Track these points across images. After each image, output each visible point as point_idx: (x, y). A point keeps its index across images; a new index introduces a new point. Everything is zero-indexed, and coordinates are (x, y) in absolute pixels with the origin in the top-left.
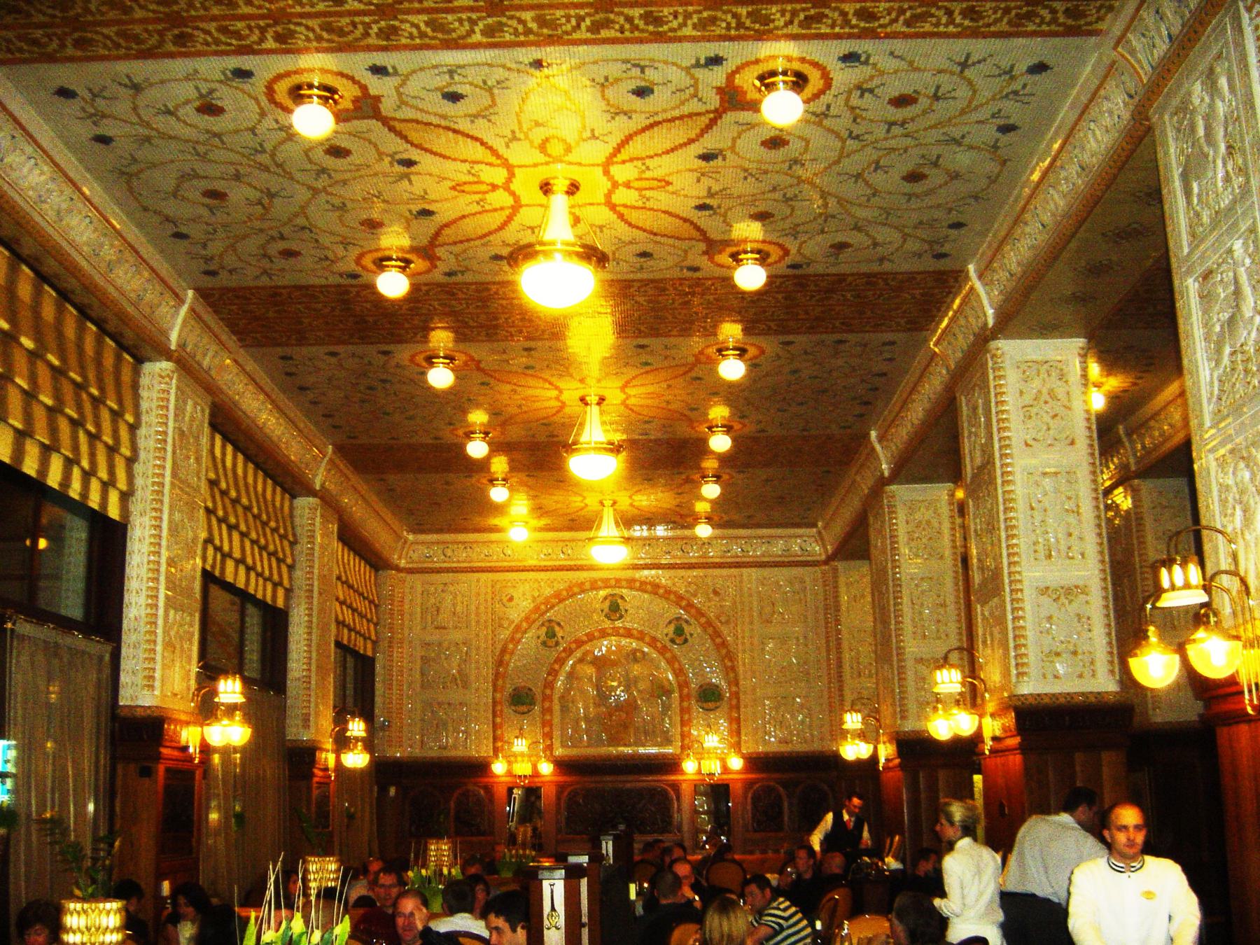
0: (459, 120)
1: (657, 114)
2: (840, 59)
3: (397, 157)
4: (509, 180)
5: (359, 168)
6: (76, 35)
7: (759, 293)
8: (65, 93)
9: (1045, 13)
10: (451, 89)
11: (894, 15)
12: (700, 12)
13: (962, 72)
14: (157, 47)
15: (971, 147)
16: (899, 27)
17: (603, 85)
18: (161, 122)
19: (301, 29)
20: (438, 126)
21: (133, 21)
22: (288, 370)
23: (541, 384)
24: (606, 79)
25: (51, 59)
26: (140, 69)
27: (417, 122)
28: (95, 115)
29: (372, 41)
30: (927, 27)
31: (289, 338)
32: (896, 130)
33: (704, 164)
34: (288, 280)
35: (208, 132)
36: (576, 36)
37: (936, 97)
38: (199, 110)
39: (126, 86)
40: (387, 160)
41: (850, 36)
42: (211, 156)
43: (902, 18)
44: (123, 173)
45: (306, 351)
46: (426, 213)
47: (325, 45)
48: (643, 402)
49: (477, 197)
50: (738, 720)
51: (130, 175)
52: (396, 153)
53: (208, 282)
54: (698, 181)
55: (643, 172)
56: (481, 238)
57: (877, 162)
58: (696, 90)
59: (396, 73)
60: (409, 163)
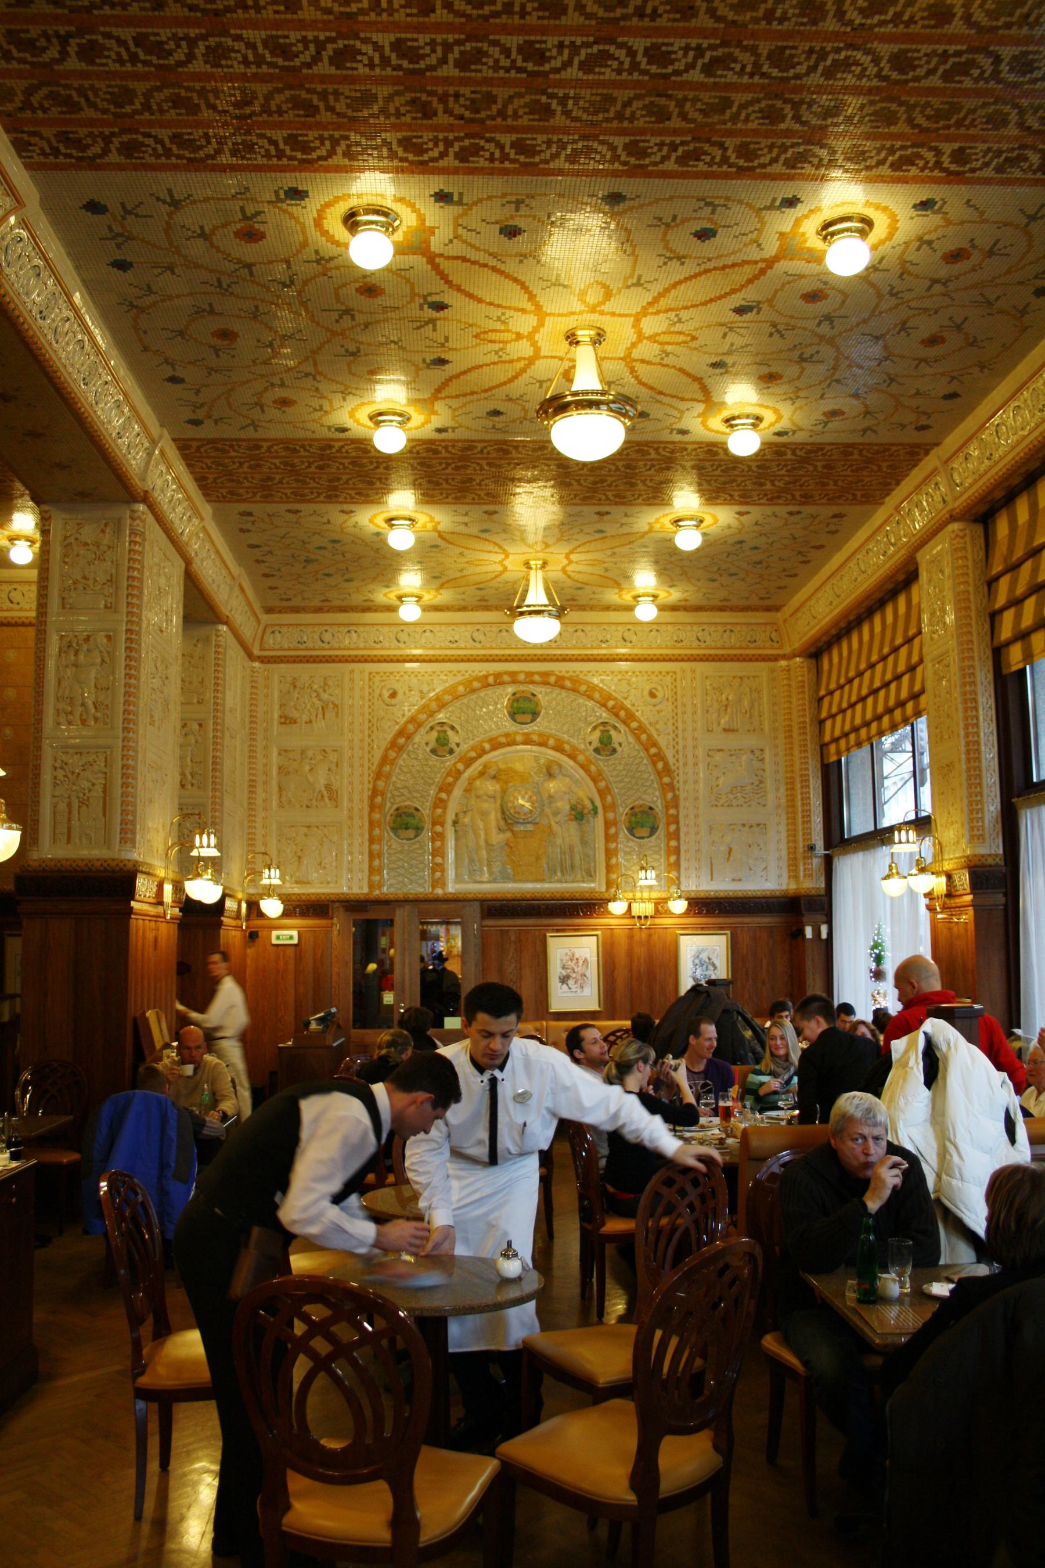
0: (508, 260)
1: (709, 260)
2: (915, 206)
3: (429, 299)
4: (536, 330)
5: (385, 309)
6: (125, 138)
7: (738, 460)
8: (94, 207)
9: (930, 155)
10: (511, 223)
11: (883, 155)
12: (575, 142)
13: (1027, 225)
14: (100, 156)
15: (1001, 312)
16: (670, 165)
17: (668, 225)
18: (197, 249)
19: (150, 141)
20: (485, 266)
21: (198, 124)
22: (245, 527)
23: (491, 547)
24: (675, 218)
25: (92, 164)
26: (180, 182)
27: (464, 259)
28: (121, 235)
29: (225, 159)
30: (701, 167)
31: (255, 494)
32: (938, 288)
33: (737, 318)
34: (275, 432)
35: (239, 261)
36: (441, 163)
37: (991, 253)
38: (237, 234)
39: (164, 202)
40: (419, 301)
41: (615, 174)
42: (236, 289)
43: (783, 157)
44: (132, 305)
45: (271, 508)
46: (442, 362)
47: (61, 159)
48: (590, 569)
49: (497, 346)
50: (677, 851)
51: (142, 310)
52: (430, 294)
53: (192, 432)
54: (447, 339)
55: (674, 324)
56: (486, 391)
57: (904, 323)
58: (759, 236)
59: (460, 203)
60: (441, 307)
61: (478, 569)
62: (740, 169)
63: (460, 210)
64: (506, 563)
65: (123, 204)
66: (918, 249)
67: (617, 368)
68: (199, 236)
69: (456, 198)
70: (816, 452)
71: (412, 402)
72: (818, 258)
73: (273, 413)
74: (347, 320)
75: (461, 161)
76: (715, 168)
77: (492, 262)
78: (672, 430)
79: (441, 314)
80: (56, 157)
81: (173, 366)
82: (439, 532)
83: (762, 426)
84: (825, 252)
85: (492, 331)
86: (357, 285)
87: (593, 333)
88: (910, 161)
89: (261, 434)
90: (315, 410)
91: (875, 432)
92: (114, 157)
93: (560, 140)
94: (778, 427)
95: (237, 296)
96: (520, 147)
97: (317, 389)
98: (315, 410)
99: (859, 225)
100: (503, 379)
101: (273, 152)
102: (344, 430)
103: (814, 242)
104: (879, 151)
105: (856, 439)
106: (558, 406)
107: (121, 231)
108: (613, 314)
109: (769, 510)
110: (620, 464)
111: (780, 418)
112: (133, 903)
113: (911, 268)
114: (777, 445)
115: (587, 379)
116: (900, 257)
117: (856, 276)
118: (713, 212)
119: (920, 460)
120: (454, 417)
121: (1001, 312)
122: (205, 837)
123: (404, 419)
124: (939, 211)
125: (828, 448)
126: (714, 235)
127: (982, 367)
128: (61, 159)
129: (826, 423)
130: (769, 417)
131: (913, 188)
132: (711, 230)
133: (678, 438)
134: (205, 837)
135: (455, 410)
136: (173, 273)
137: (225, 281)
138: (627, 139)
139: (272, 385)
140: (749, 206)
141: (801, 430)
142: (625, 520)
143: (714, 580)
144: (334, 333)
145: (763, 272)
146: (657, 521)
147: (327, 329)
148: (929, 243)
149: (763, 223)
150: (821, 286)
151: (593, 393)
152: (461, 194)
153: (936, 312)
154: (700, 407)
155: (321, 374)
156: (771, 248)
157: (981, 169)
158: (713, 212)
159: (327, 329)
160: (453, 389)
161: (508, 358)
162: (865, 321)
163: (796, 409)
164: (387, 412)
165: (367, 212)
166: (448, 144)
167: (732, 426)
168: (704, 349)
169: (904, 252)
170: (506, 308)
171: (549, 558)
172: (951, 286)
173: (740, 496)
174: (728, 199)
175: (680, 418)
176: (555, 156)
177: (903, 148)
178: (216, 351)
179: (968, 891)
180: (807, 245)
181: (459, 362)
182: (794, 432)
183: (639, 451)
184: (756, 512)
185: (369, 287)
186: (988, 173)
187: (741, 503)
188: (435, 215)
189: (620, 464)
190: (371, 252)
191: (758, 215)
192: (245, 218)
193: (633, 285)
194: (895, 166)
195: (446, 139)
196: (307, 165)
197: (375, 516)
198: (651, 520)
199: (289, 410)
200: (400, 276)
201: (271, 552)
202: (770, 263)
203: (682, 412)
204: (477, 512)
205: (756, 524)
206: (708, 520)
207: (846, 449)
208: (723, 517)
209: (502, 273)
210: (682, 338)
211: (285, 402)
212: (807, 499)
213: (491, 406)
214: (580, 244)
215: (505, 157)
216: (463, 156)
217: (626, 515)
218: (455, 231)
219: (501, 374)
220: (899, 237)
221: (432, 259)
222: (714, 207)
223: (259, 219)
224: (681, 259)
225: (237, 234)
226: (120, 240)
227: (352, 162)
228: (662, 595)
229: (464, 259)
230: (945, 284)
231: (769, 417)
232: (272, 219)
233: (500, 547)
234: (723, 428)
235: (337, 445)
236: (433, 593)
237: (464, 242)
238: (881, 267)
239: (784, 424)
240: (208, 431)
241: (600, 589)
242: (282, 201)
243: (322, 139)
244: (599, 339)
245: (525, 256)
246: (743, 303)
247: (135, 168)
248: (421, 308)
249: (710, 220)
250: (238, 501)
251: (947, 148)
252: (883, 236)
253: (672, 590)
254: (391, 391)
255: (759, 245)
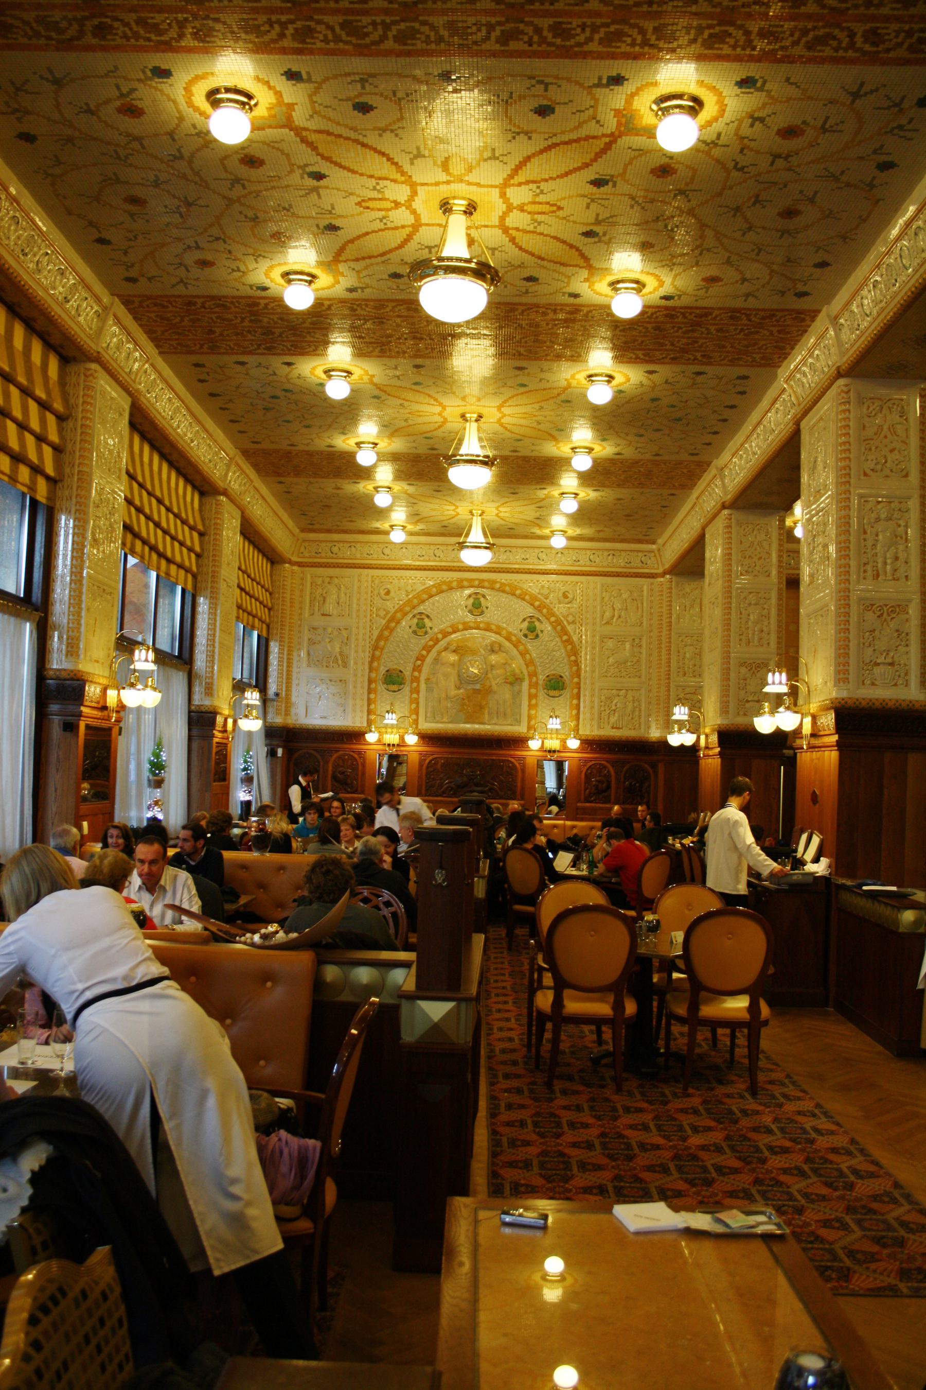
3: (308, 169)
13: (853, 102)
22: (202, 377)
23: (427, 400)
27: (329, 133)
31: (202, 346)
32: (780, 163)
38: (120, 110)
48: (523, 422)
52: (307, 165)
57: (758, 196)
58: (595, 112)
59: (309, 80)
60: (319, 176)
61: (420, 420)
62: (865, 53)
63: (310, 87)
64: (445, 414)
65: (13, 83)
66: (752, 126)
67: (494, 236)
68: (86, 112)
69: (305, 76)
70: (706, 315)
71: (320, 264)
72: (650, 133)
73: (196, 272)
74: (238, 188)
75: (502, 45)
76: (841, 53)
77: (353, 135)
78: (564, 294)
79: (322, 183)
80: (137, 40)
81: (97, 228)
82: (376, 385)
83: (645, 291)
84: (655, 127)
85: (370, 199)
86: (239, 156)
87: (465, 203)
88: (821, 41)
89: (192, 291)
90: (233, 270)
91: (186, 284)
92: (90, 39)
93: (593, 24)
94: (662, 292)
95: (136, 167)
96: (557, 30)
97: (230, 252)
98: (233, 270)
99: (691, 104)
100: (393, 245)
101: (330, 37)
102: (265, 289)
103: (648, 119)
104: (898, 33)
105: (739, 303)
106: (425, 267)
107: (16, 106)
108: (478, 185)
109: (677, 368)
110: (650, 326)
111: (661, 284)
112: (83, 708)
113: (752, 144)
114: (667, 308)
115: (456, 247)
116: (736, 134)
117: (691, 149)
118: (546, 90)
119: (809, 326)
120: (359, 278)
121: (848, 185)
122: (144, 652)
123: (640, 285)
124: (761, 89)
125: (716, 312)
126: (553, 112)
127: (844, 238)
128: (142, 42)
129: (708, 289)
130: (651, 283)
131: (735, 65)
132: (549, 106)
133: (572, 300)
134: (777, 674)
135: (358, 272)
136: (74, 145)
137: (122, 153)
138: (551, 21)
139: (189, 247)
140: (581, 85)
141: (685, 294)
142: (542, 375)
143: (641, 436)
144: (230, 202)
145: (608, 147)
146: (573, 376)
147: (224, 197)
148: (762, 120)
149: (597, 100)
150: (667, 160)
151: (459, 260)
152: (308, 73)
153: (785, 186)
154: (585, 273)
155: (229, 238)
156: (611, 124)
157: (894, 49)
158: (546, 90)
159: (224, 197)
160: (350, 251)
161: (392, 225)
162: (720, 194)
163: (676, 276)
164: (296, 274)
165: (228, 90)
166: (284, 26)
167: (616, 290)
168: (571, 218)
169: (738, 128)
170: (380, 179)
171: (484, 411)
172: (794, 161)
173: (644, 355)
174: (557, 77)
175: (568, 284)
176: (590, 40)
177: (814, 28)
178: (132, 215)
179: (833, 731)
180: (644, 123)
181: (350, 228)
182: (680, 296)
183: (731, 318)
184: (664, 371)
185: (248, 157)
186: (901, 53)
187: (647, 362)
188: (292, 93)
189: (650, 326)
190: (230, 128)
191: (589, 93)
192: (122, 95)
193: (490, 158)
194: (708, 44)
195: (383, 22)
196: (168, 47)
197: (314, 368)
198: (567, 374)
199: (207, 270)
200: (273, 147)
201: (230, 401)
202: (613, 138)
203: (569, 277)
204: (405, 364)
205: (666, 382)
206: (619, 379)
207: (734, 314)
208: (631, 376)
209: (364, 145)
210: (546, 208)
211: (204, 264)
212: (707, 359)
213: (392, 269)
214: (459, 118)
215: (543, 40)
216: (401, 38)
217: (542, 370)
218: (313, 108)
219: (396, 238)
220: (729, 115)
221: (298, 131)
222: (546, 86)
223: (134, 96)
224: (528, 134)
225: (120, 110)
226: (18, 115)
227: (206, 43)
228: (597, 448)
229: (329, 133)
230: (786, 158)
231: (651, 283)
232: (145, 96)
233: (436, 400)
234: (607, 290)
235: (263, 302)
236: (386, 440)
237: (324, 117)
238: (720, 143)
239: (667, 289)
240: (143, 287)
241: (538, 441)
242: (150, 79)
243: (374, 24)
244: (471, 209)
245: (384, 130)
246: (597, 176)
247: (409, 54)
248: (302, 178)
249: (545, 97)
250: (188, 353)
251: (860, 28)
252: (715, 114)
253: (604, 444)
254: (303, 254)
255: (598, 122)
